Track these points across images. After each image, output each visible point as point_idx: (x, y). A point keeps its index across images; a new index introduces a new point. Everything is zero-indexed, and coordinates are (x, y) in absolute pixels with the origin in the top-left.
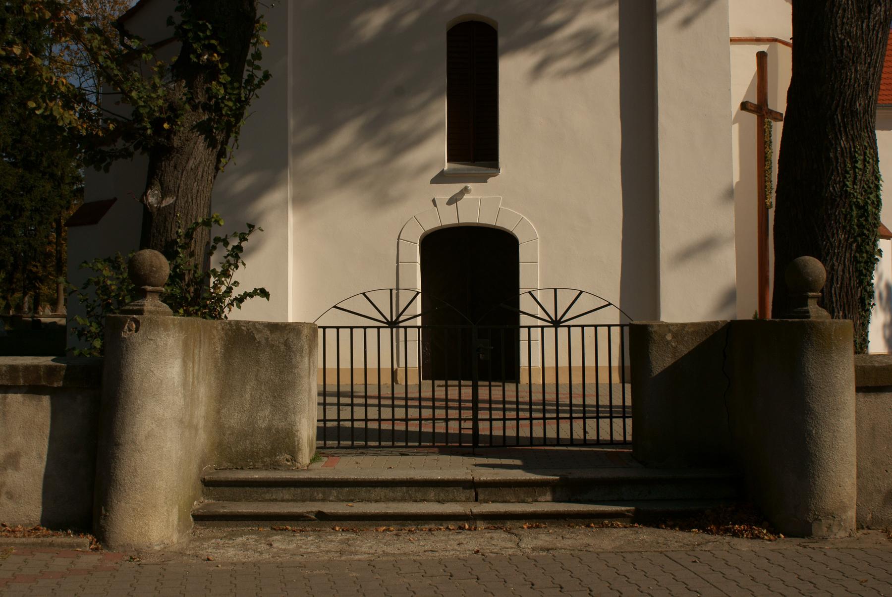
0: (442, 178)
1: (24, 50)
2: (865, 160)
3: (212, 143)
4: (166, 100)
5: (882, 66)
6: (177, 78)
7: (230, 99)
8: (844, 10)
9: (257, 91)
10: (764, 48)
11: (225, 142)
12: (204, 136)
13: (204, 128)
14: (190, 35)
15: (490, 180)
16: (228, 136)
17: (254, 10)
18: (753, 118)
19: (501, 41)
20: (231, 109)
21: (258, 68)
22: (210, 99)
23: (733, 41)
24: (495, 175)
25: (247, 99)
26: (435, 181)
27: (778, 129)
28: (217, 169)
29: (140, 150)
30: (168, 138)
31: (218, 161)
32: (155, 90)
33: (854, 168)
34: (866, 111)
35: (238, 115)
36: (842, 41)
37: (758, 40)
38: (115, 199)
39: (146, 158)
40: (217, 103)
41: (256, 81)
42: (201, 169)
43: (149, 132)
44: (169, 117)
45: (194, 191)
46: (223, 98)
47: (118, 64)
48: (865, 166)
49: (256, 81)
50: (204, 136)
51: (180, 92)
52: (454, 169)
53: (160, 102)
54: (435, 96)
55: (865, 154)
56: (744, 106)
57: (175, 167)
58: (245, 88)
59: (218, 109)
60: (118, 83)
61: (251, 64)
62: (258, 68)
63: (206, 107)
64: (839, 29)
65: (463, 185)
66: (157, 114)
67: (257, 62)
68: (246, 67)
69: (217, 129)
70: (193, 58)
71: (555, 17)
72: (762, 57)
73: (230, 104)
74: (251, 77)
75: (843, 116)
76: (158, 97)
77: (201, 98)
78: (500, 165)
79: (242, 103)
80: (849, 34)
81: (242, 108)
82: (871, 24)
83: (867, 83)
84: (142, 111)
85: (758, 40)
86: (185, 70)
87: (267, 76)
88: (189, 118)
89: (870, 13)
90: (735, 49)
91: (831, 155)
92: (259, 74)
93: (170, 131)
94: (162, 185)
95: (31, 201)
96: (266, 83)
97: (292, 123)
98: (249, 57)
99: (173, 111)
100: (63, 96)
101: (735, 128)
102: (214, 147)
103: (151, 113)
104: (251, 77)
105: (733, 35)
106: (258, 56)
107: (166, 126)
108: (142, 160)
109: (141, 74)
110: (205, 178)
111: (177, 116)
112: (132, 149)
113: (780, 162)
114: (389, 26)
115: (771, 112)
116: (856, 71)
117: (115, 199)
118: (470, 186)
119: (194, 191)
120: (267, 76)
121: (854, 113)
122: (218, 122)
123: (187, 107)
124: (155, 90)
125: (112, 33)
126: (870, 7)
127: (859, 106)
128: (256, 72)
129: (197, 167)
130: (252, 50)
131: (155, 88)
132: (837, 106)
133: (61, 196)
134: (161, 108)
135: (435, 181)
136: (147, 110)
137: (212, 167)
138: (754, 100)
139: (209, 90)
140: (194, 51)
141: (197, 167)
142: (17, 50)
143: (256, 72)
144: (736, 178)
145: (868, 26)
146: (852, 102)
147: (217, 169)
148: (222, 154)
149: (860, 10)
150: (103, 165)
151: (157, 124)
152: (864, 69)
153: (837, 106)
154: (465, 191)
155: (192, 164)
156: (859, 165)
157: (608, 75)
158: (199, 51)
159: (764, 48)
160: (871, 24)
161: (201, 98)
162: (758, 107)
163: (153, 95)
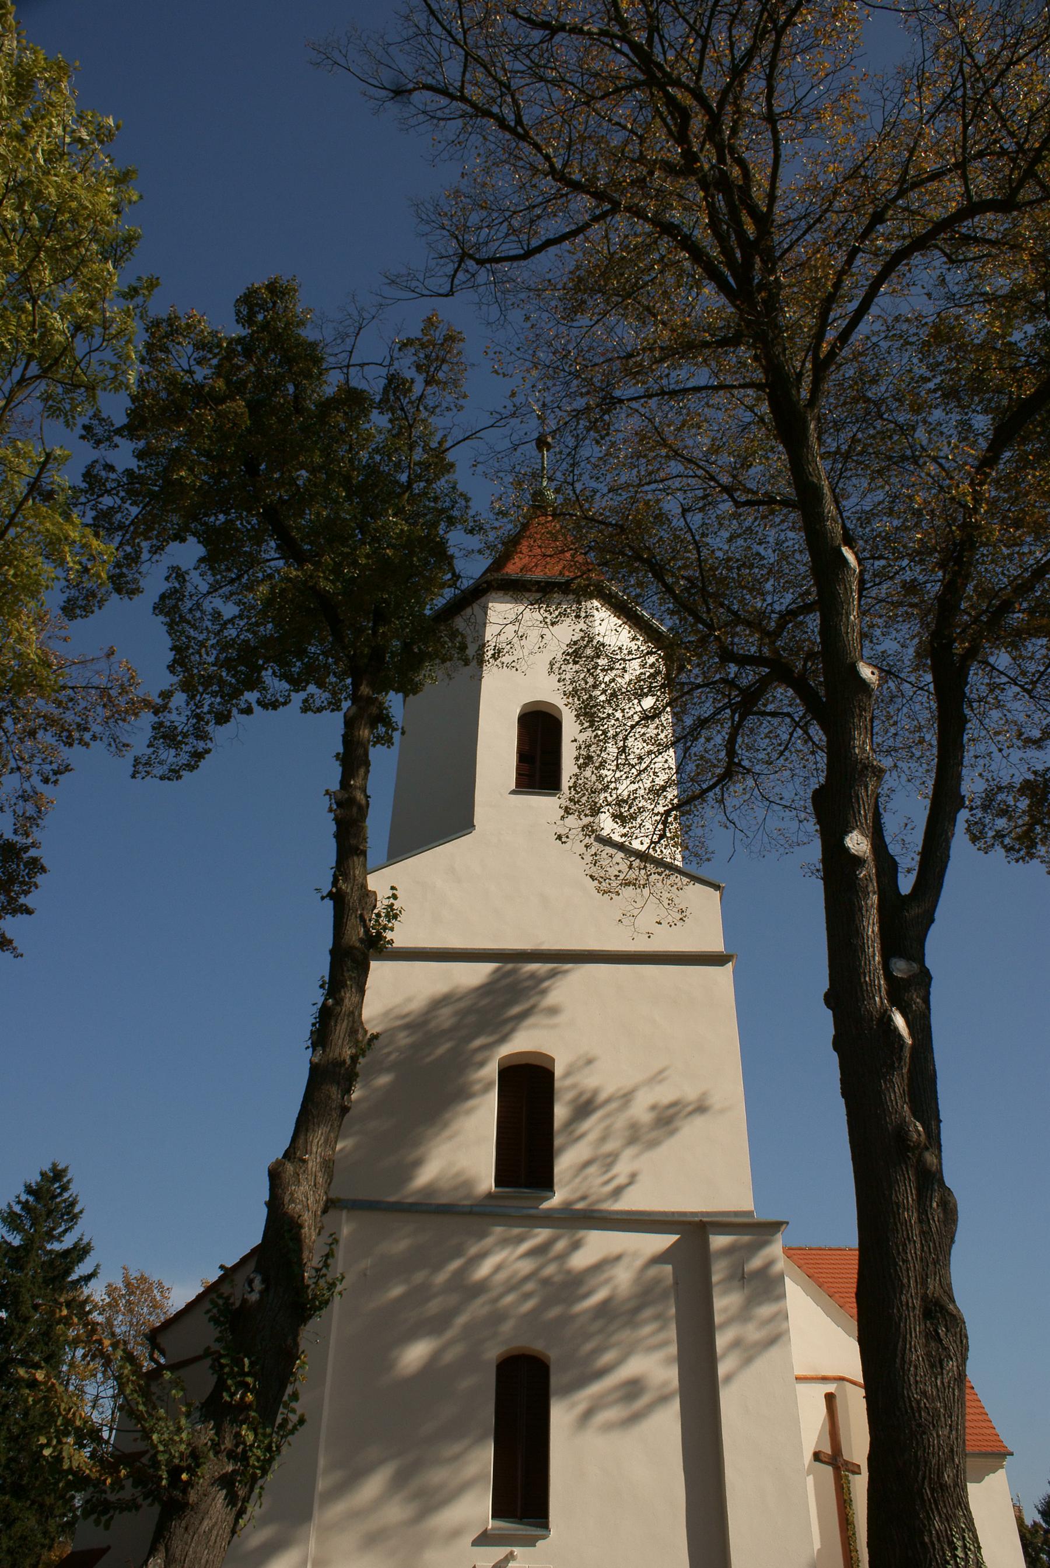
0: (484, 1539)
1: (47, 1376)
2: (965, 1547)
3: (232, 1499)
4: (189, 1444)
5: (964, 1428)
6: (205, 1419)
7: (258, 1447)
8: (916, 1367)
9: (290, 1438)
10: (831, 1388)
11: (246, 1499)
12: (224, 1492)
13: (226, 1482)
14: (227, 1370)
15: (540, 1543)
16: (251, 1490)
17: (296, 1345)
18: (829, 1470)
19: (555, 1381)
20: (258, 1459)
21: (293, 1411)
22: (237, 1446)
23: (799, 1379)
24: (544, 1537)
25: (278, 1448)
26: (476, 1543)
27: (860, 1485)
28: (233, 1532)
29: (149, 1500)
30: (185, 1492)
31: (236, 1522)
32: (178, 1433)
33: (955, 1556)
34: (956, 1485)
35: (265, 1467)
36: (918, 1402)
37: (825, 1379)
38: (109, 1548)
39: (157, 1508)
40: (244, 1451)
41: (290, 1426)
42: (215, 1532)
43: (164, 1482)
44: (189, 1466)
45: (203, 1561)
46: (252, 1446)
47: (141, 1393)
48: (966, 1554)
49: (290, 1426)
50: (224, 1492)
51: (206, 1434)
52: (500, 1529)
53: (183, 1447)
54: (480, 1440)
55: (964, 1538)
56: (817, 1456)
57: (186, 1529)
58: (277, 1433)
59: (244, 1458)
60: (139, 1418)
61: (286, 1406)
62: (293, 1411)
63: (231, 1455)
64: (913, 1387)
65: (508, 1549)
66: (177, 1461)
67: (293, 1405)
68: (281, 1410)
69: (240, 1482)
70: (226, 1397)
71: (608, 1357)
72: (830, 1398)
73: (259, 1453)
74: (285, 1420)
75: (932, 1490)
76: (181, 1441)
77: (228, 1443)
78: (551, 1525)
79: (272, 1451)
80: (924, 1393)
81: (271, 1460)
82: (946, 1381)
83: (952, 1451)
84: (161, 1457)
85: (825, 1379)
86: (215, 1410)
87: (302, 1421)
88: (214, 1467)
89: (942, 1368)
90: (802, 1388)
91: (926, 1539)
92: (294, 1418)
93: (189, 1484)
94: (167, 1551)
95: (10, 1538)
96: (301, 1429)
97: (322, 1462)
98: (285, 1398)
99: (195, 1456)
100: (78, 1430)
101: (810, 1480)
102: (234, 1505)
103: (169, 1462)
104: (285, 1420)
105: (799, 1372)
106: (295, 1397)
107: (184, 1476)
108: (151, 1512)
109: (167, 1412)
110: (218, 1544)
111: (198, 1466)
112: (140, 1500)
113: (869, 1545)
114: (434, 1358)
115: (847, 1463)
116: (938, 1436)
117: (109, 1548)
118: (517, 1550)
119: (203, 1561)
120: (302, 1421)
121: (943, 1487)
122: (243, 1474)
123: (211, 1454)
124: (178, 1433)
125: (140, 1351)
126: (941, 1361)
127: (947, 1477)
128: (291, 1415)
129: (211, 1530)
130: (289, 1390)
131: (179, 1430)
132: (924, 1478)
133: (45, 1533)
134: (182, 1453)
135: (476, 1543)
136: (167, 1456)
137: (228, 1530)
138: (827, 1449)
139: (238, 1434)
140: (228, 1389)
141: (211, 1530)
142: (40, 1376)
143: (291, 1415)
144: (817, 1545)
145: (942, 1383)
146: (940, 1475)
147: (233, 1532)
148: (240, 1514)
149: (932, 1366)
150: (104, 1519)
151: (175, 1473)
152: (946, 1432)
153: (924, 1478)
154: (510, 1557)
155: (206, 1525)
156: (960, 1553)
157: (667, 1425)
158: (233, 1389)
159: (831, 1388)
160: (946, 1381)
161: (228, 1443)
162: (831, 1456)
163: (177, 1438)
